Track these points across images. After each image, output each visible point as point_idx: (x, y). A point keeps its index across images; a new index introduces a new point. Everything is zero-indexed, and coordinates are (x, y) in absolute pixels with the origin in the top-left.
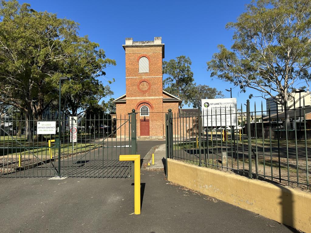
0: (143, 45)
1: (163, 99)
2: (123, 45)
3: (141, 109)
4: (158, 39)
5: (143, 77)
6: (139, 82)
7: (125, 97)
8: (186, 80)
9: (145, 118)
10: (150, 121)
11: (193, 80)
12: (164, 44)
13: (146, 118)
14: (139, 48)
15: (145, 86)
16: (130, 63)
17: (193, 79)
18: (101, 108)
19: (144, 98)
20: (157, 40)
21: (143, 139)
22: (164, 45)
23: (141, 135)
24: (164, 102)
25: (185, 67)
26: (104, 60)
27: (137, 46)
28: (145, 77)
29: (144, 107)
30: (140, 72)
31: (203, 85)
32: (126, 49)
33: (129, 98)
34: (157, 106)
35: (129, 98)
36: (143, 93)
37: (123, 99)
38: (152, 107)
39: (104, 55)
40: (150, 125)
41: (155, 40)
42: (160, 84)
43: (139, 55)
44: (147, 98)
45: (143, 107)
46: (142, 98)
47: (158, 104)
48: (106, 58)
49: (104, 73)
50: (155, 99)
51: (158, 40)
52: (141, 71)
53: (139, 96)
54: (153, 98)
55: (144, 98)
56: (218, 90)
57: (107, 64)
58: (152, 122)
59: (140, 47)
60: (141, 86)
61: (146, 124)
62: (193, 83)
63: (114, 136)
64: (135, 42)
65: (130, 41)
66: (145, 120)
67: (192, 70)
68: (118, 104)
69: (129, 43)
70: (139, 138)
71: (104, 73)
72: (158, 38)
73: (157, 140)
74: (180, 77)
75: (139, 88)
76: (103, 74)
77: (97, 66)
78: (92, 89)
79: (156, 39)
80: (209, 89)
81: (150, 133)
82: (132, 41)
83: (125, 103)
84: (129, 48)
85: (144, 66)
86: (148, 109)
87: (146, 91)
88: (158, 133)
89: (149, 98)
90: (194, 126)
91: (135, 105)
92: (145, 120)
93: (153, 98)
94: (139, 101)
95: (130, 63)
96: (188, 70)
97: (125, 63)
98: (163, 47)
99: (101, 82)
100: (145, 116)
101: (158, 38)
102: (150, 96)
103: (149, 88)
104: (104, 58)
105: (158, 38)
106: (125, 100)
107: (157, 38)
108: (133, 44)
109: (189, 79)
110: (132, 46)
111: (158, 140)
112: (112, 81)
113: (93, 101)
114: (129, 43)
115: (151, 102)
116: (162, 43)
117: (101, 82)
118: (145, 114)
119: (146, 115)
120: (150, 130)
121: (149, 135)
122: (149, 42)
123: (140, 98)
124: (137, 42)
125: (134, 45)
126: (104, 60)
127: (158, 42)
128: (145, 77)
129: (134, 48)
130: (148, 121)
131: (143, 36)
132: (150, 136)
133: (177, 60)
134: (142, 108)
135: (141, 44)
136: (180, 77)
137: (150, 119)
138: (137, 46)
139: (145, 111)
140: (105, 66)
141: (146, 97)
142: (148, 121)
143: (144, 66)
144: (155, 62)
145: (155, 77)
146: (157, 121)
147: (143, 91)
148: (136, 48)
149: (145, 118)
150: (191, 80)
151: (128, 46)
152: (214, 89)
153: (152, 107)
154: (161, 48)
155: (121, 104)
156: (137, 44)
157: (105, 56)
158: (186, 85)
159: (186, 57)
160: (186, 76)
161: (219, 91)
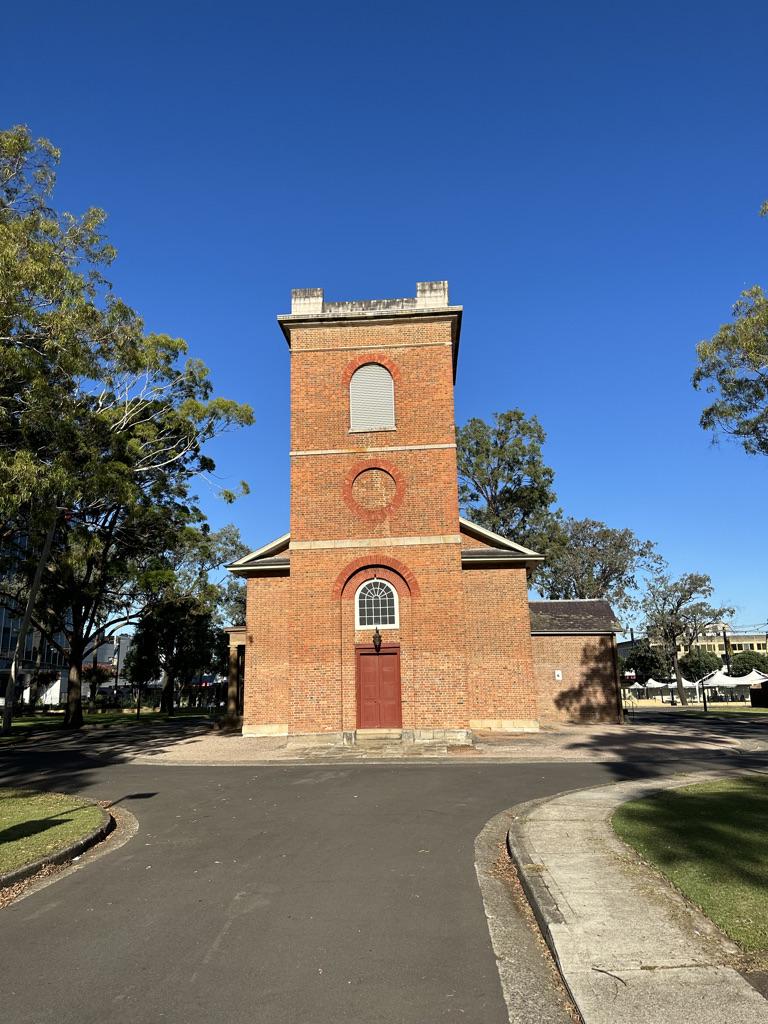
0: (369, 314)
1: (464, 555)
2: (281, 317)
3: (361, 596)
4: (432, 289)
5: (369, 449)
6: (353, 470)
7: (284, 546)
8: (530, 499)
9: (377, 637)
10: (404, 656)
11: (553, 499)
12: (459, 308)
13: (384, 642)
14: (349, 329)
15: (378, 489)
16: (312, 390)
17: (551, 496)
18: (189, 604)
19: (374, 543)
20: (428, 294)
21: (373, 744)
22: (459, 313)
23: (359, 725)
24: (466, 566)
25: (524, 448)
26: (204, 404)
27: (340, 321)
28: (378, 449)
29: (376, 584)
30: (354, 428)
31: (579, 519)
32: (294, 333)
33: (306, 545)
34: (434, 579)
35: (306, 545)
36: (370, 519)
37: (277, 557)
38: (409, 586)
39: (208, 386)
40: (406, 676)
41: (419, 294)
42: (446, 478)
43: (350, 359)
44: (388, 544)
45: (369, 586)
46: (364, 543)
47: (439, 571)
48: (215, 398)
49: (207, 465)
50: (423, 548)
51: (433, 294)
52: (356, 426)
53: (350, 536)
54: (416, 541)
55: (374, 543)
56: (640, 536)
57: (219, 424)
58: (414, 658)
59: (353, 325)
60: (359, 491)
61: (385, 670)
62: (552, 508)
63: (231, 725)
64: (333, 304)
65: (313, 300)
66: (378, 648)
67: (546, 461)
68: (255, 580)
69: (306, 306)
70: (349, 739)
71: (207, 465)
72: (431, 286)
73: (445, 754)
74: (501, 485)
75: (349, 499)
76: (202, 468)
77: (177, 431)
78: (155, 534)
79: (423, 291)
80: (605, 535)
81: (406, 711)
82: (320, 300)
83: (285, 573)
84: (307, 331)
85: (371, 402)
86: (391, 595)
87: (382, 512)
88: (442, 713)
89: (395, 543)
90: (591, 676)
91: (334, 579)
92: (378, 648)
93: (416, 541)
94: (351, 557)
95: (312, 390)
96: (532, 463)
97: (288, 391)
98: (457, 320)
99: (196, 498)
100: (381, 627)
101: (435, 286)
102: (400, 534)
103: (398, 500)
104: (206, 396)
105: (431, 286)
106: (287, 562)
107: (427, 287)
108: (323, 311)
109: (536, 494)
110: (321, 321)
111: (452, 755)
112: (236, 489)
113: (157, 575)
114: (306, 306)
115: (404, 561)
116: (449, 304)
117: (196, 498)
118: (377, 621)
119: (384, 622)
120: (404, 698)
121: (400, 725)
122: (394, 303)
123: (356, 544)
124: (344, 304)
125: (328, 314)
126: (204, 404)
127: (434, 299)
128: (378, 449)
129: (328, 330)
130: (394, 651)
131: (369, 279)
132: (407, 726)
133: (494, 425)
134: (364, 590)
135: (357, 312)
136: (501, 485)
137: (402, 643)
138: (340, 321)
139: (377, 603)
140: (210, 429)
141: (381, 536)
142: (394, 651)
143: (371, 402)
144: (423, 384)
145: (422, 447)
146: (435, 651)
147: (370, 512)
148: (338, 329)
149: (377, 637)
150: (544, 498)
151: (301, 322)
152: (627, 533)
153: (409, 586)
154: (449, 324)
155: (269, 579)
156: (342, 312)
157: (212, 389)
158: (526, 514)
159: (527, 418)
160: (526, 482)
161: (644, 540)
